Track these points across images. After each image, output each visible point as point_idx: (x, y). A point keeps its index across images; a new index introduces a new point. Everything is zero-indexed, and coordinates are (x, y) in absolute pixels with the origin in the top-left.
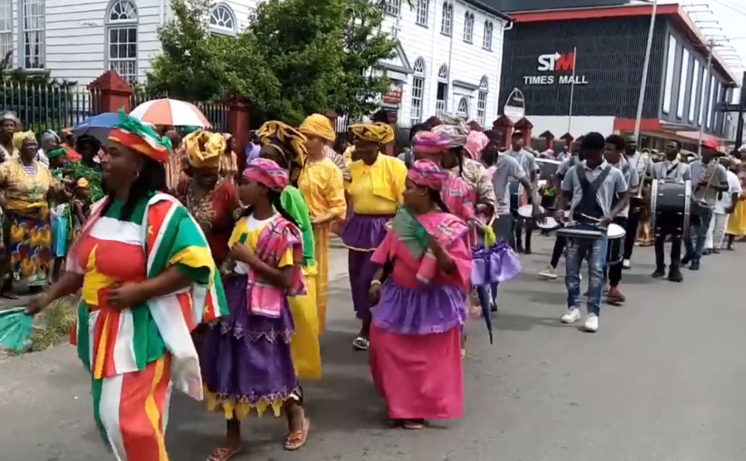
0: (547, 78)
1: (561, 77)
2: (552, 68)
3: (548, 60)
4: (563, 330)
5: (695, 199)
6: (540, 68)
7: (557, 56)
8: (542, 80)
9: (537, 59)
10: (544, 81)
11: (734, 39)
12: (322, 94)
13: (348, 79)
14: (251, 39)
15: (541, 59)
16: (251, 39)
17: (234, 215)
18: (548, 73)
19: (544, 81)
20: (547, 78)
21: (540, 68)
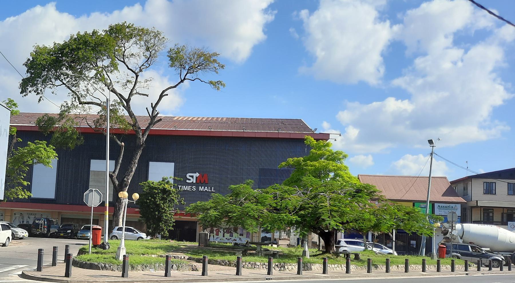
0: (192, 187)
1: (200, 187)
2: (195, 182)
3: (192, 177)
4: (447, 246)
5: (165, 230)
6: (188, 181)
7: (197, 175)
8: (189, 188)
9: (186, 175)
10: (190, 189)
11: (463, 168)
12: (311, 138)
13: (40, 120)
14: (339, 213)
15: (188, 176)
16: (339, 213)
17: (350, 104)
18: (192, 184)
19: (190, 189)
20: (192, 187)
21: (188, 181)
